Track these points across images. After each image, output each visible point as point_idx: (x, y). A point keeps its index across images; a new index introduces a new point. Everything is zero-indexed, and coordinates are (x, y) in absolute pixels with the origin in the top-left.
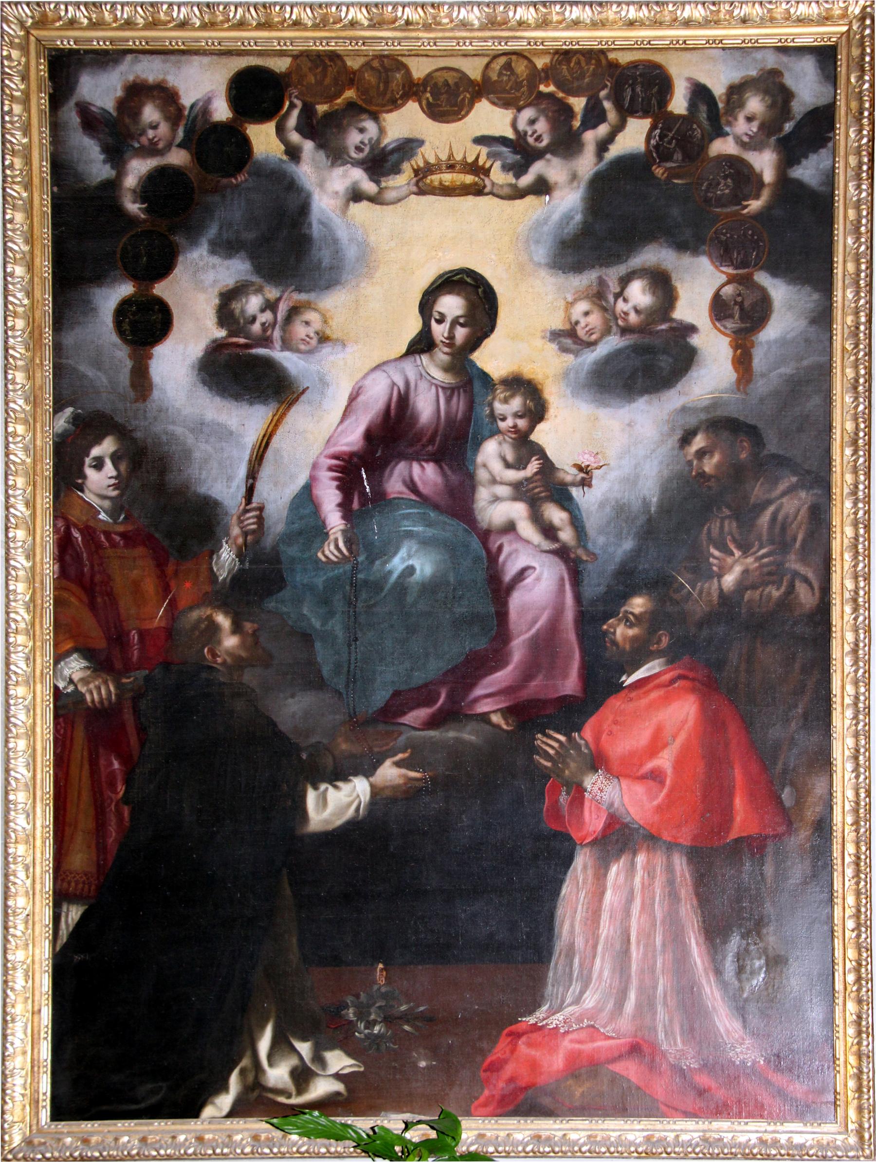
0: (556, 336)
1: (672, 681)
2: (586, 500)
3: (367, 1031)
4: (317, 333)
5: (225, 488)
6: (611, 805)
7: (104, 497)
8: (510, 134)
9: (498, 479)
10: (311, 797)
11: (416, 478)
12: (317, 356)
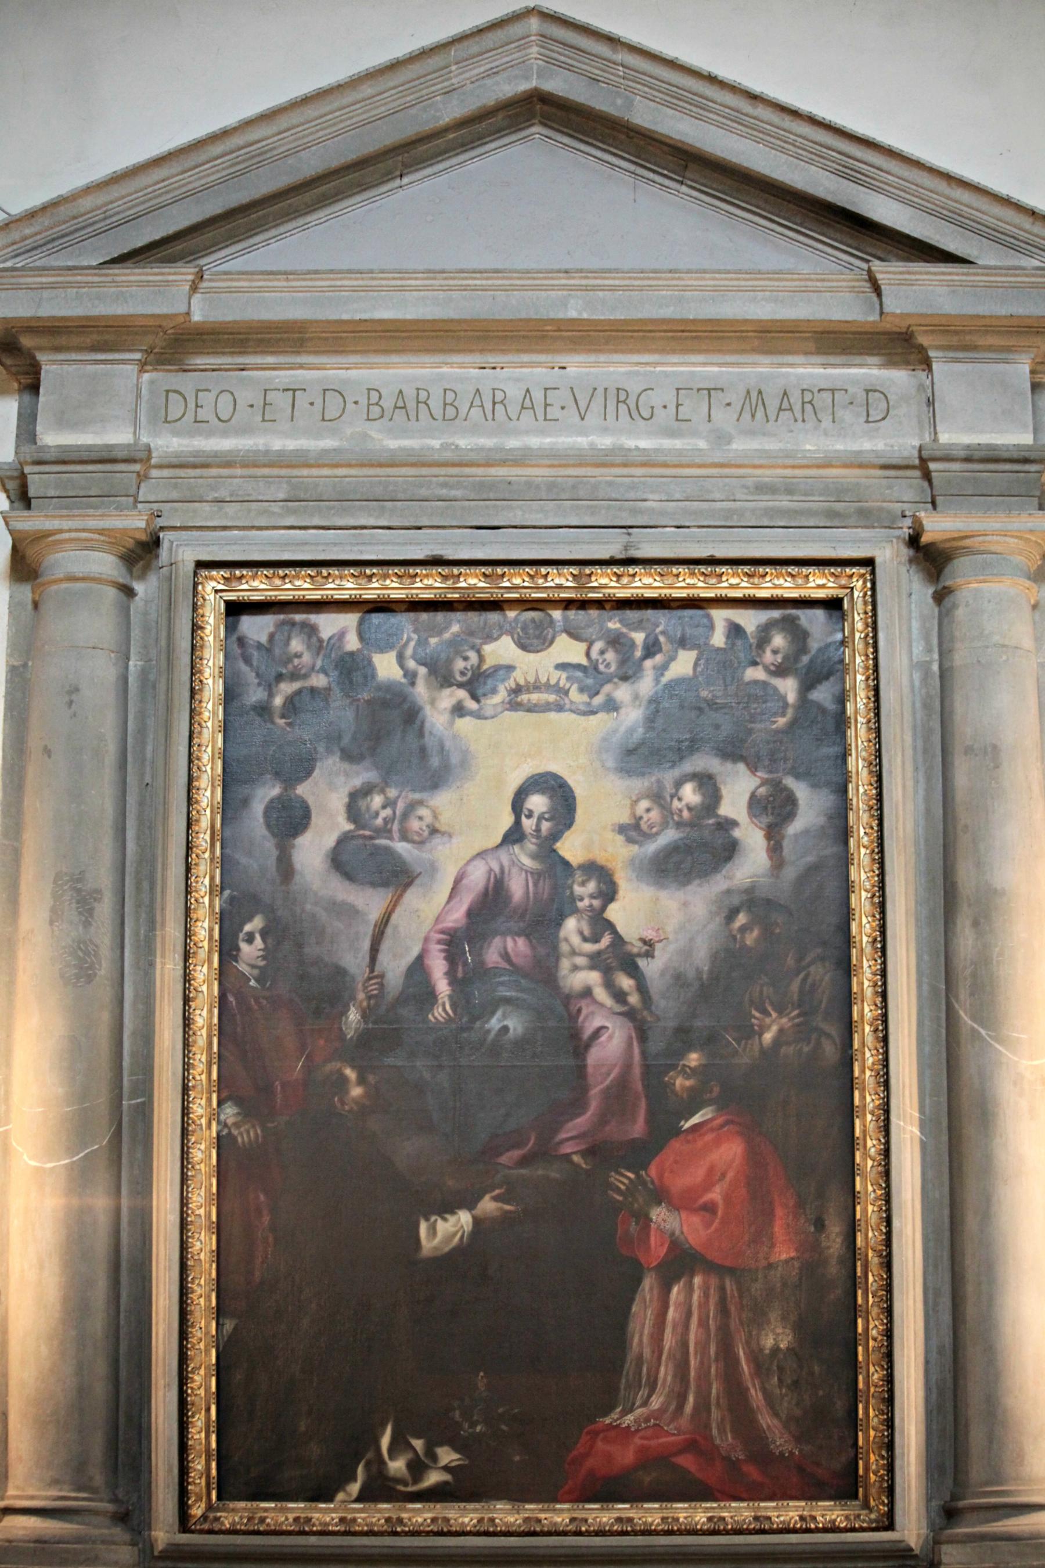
0: (622, 829)
1: (722, 1126)
2: (651, 968)
3: (471, 1430)
4: (428, 826)
5: (354, 960)
6: (673, 1234)
7: (253, 967)
8: (584, 662)
9: (577, 951)
10: (423, 1227)
11: (510, 950)
12: (428, 846)
